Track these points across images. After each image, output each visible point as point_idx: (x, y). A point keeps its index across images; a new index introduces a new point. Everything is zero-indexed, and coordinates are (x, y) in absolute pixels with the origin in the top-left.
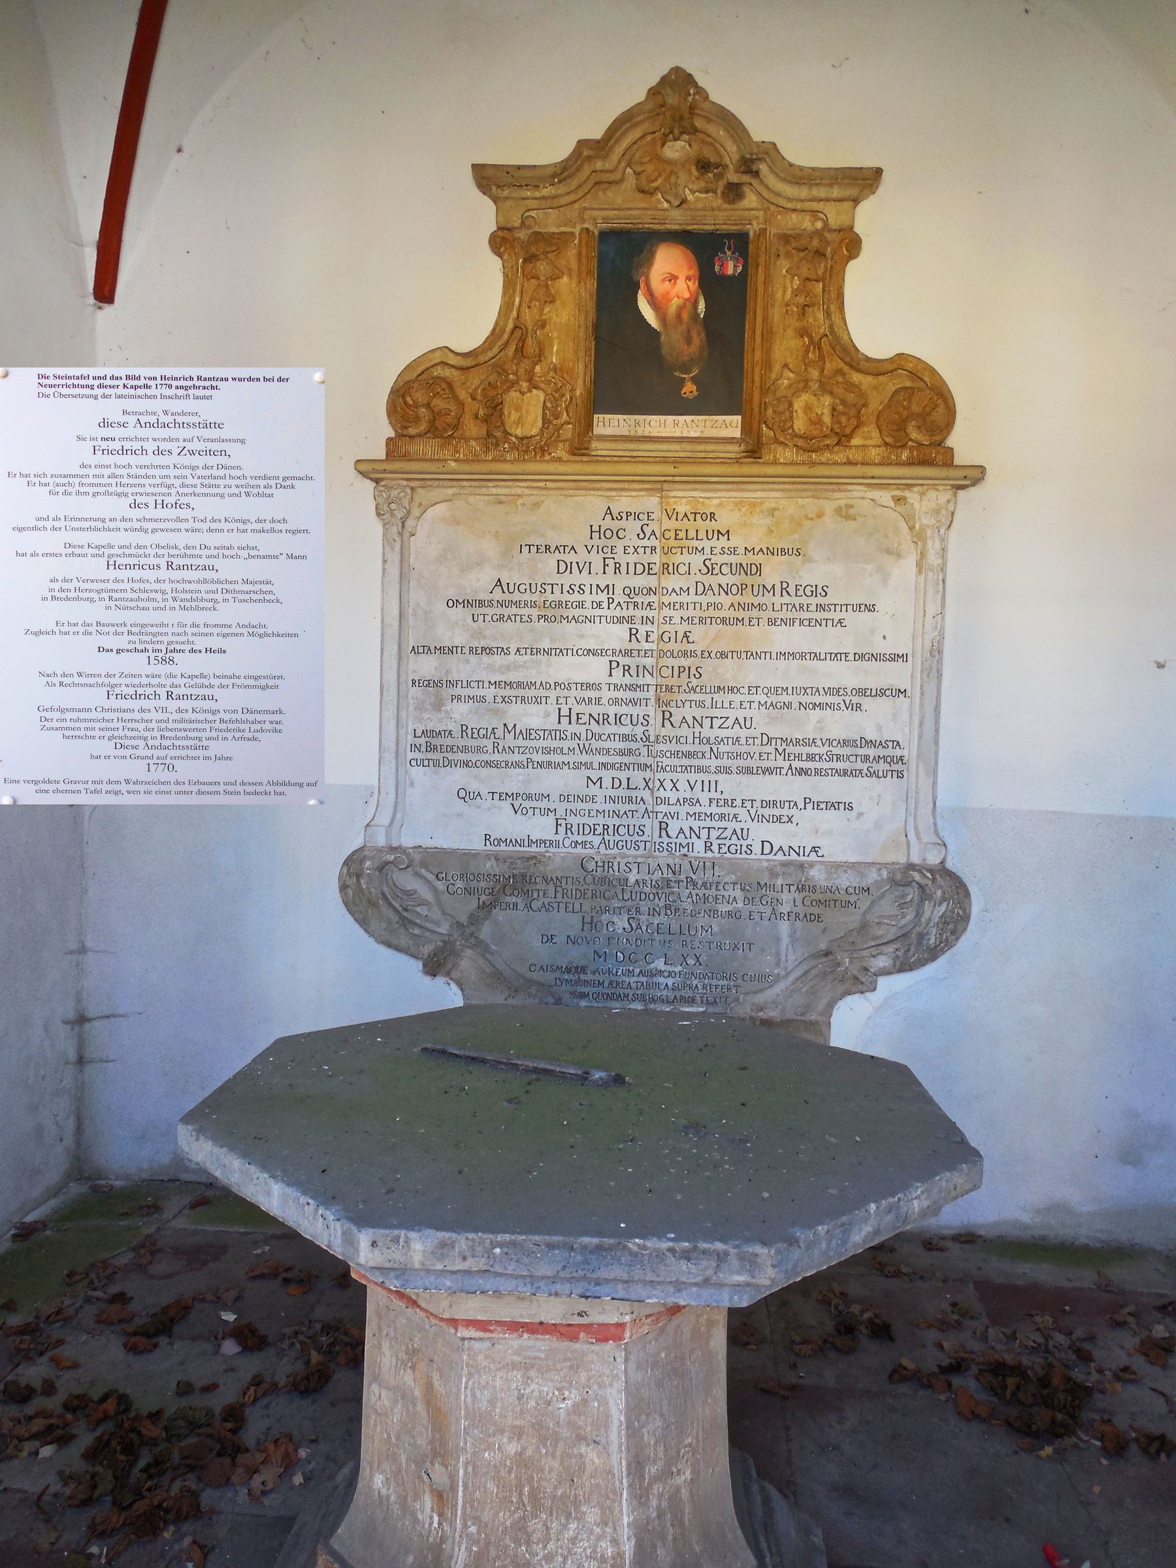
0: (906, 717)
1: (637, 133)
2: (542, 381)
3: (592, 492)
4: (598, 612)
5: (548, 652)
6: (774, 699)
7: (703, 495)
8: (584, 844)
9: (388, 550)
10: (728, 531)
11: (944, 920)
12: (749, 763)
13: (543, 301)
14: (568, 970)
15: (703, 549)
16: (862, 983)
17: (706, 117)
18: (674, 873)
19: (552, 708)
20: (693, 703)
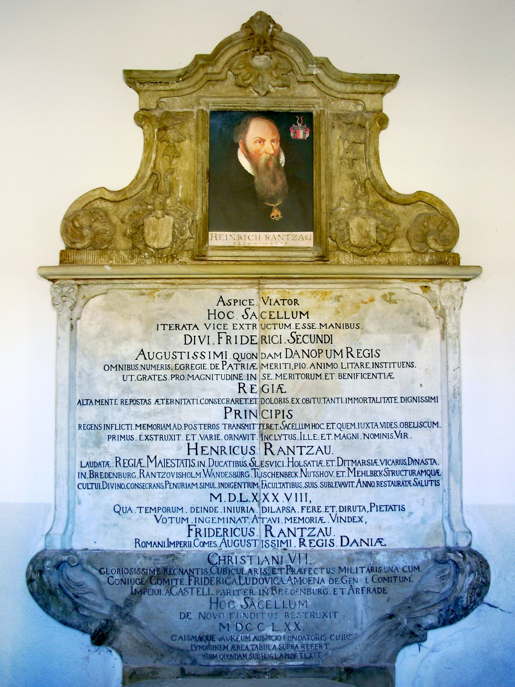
0: (439, 442)
1: (235, 51)
2: (171, 210)
3: (208, 286)
4: (215, 372)
5: (179, 402)
6: (345, 432)
7: (288, 287)
8: (210, 543)
9: (60, 330)
10: (307, 312)
11: (473, 587)
12: (330, 479)
13: (171, 156)
14: (201, 639)
15: (290, 325)
16: (417, 636)
17: (282, 42)
18: (277, 563)
19: (183, 443)
20: (287, 436)
